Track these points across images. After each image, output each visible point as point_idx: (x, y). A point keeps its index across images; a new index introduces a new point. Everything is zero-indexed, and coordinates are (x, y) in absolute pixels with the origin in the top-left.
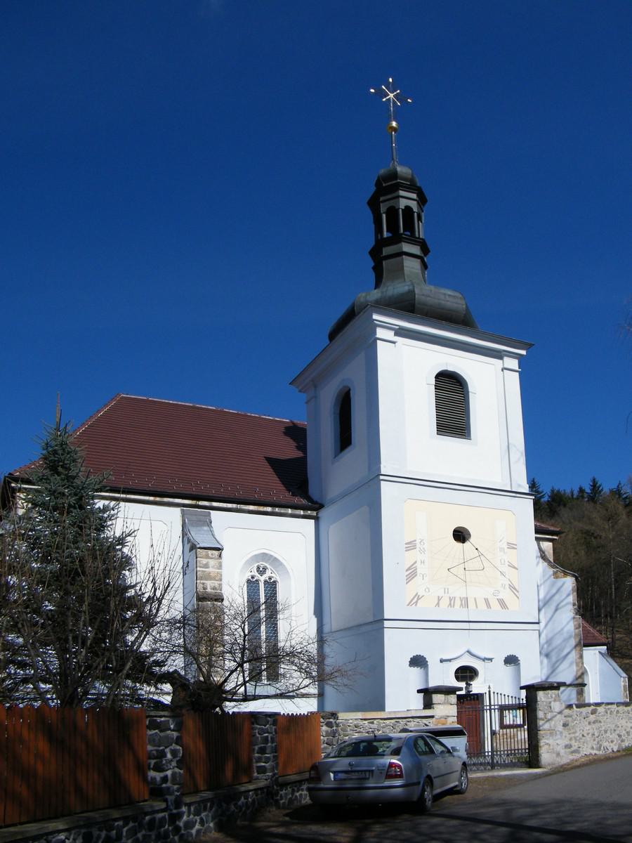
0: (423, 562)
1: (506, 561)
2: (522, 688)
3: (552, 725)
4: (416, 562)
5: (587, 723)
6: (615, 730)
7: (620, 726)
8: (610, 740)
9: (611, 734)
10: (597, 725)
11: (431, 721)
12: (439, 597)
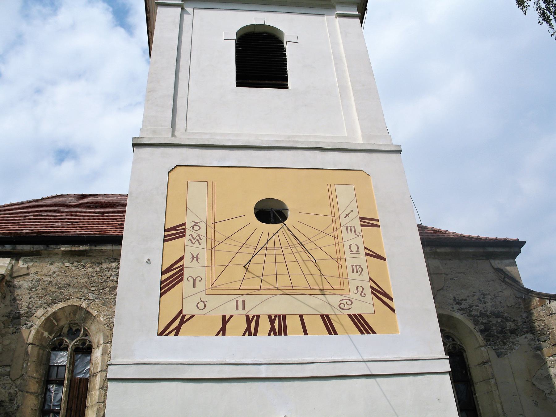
4: (182, 258)
12: (224, 317)
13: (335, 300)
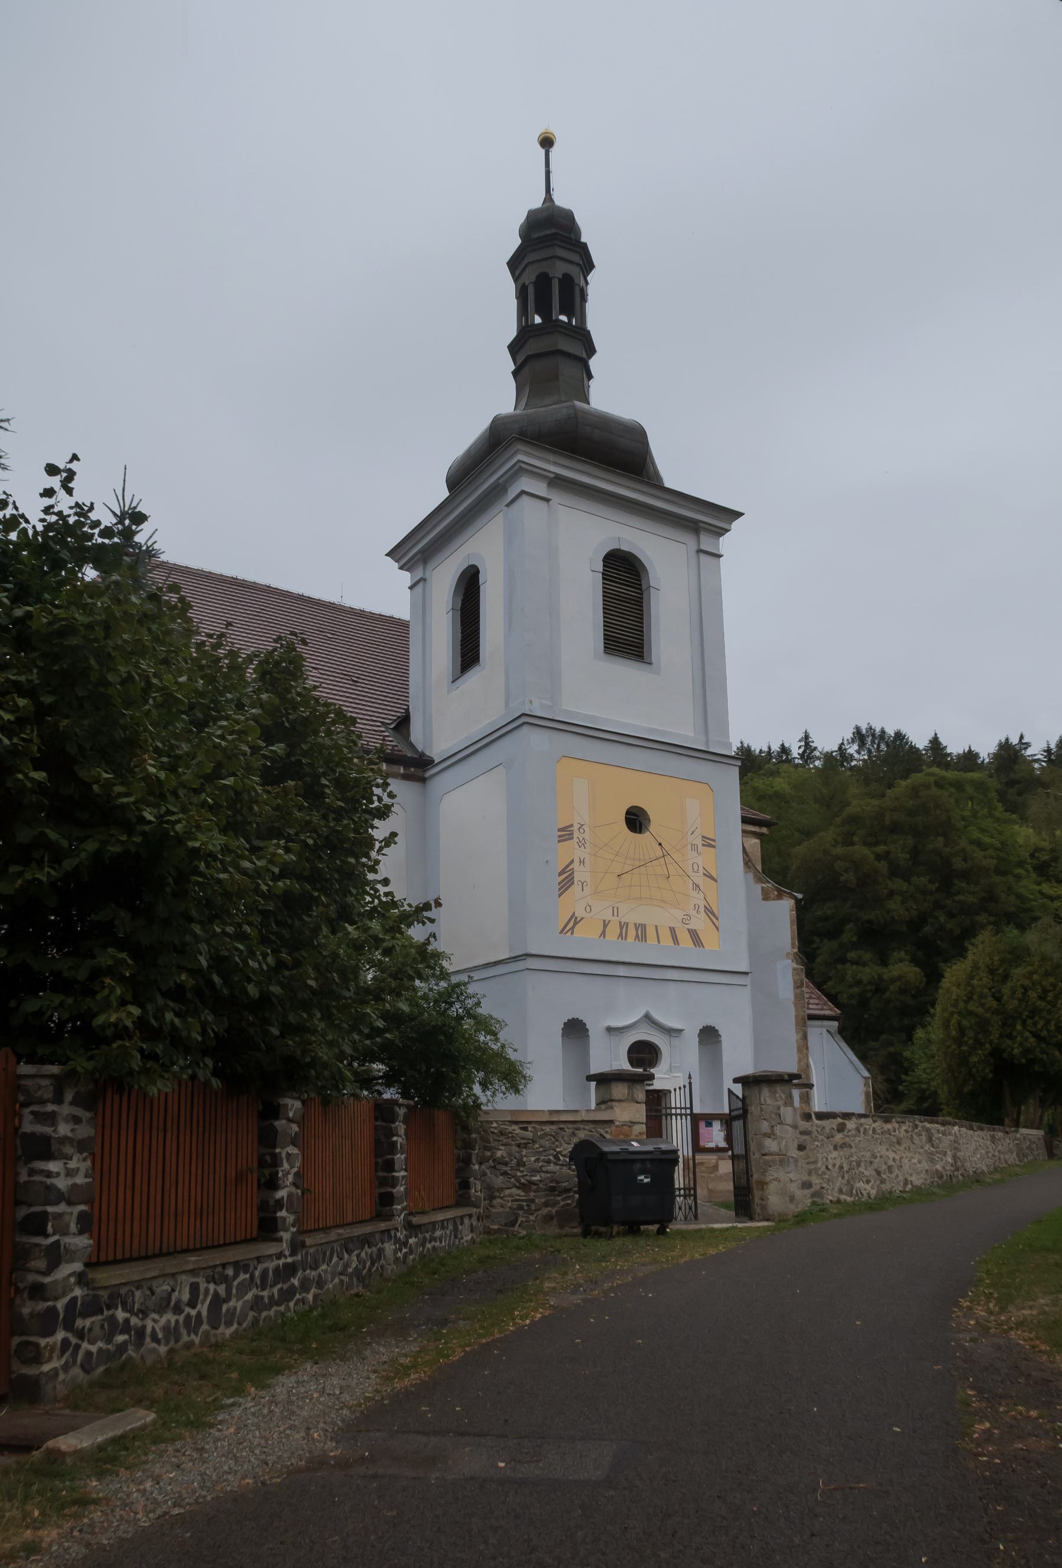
0: (582, 862)
1: (701, 868)
2: (590, 1078)
3: (782, 1147)
4: (572, 861)
5: (832, 1147)
6: (871, 1163)
7: (878, 1155)
8: (865, 1179)
9: (866, 1169)
10: (846, 1152)
11: (609, 1130)
12: (604, 921)
13: (679, 914)
